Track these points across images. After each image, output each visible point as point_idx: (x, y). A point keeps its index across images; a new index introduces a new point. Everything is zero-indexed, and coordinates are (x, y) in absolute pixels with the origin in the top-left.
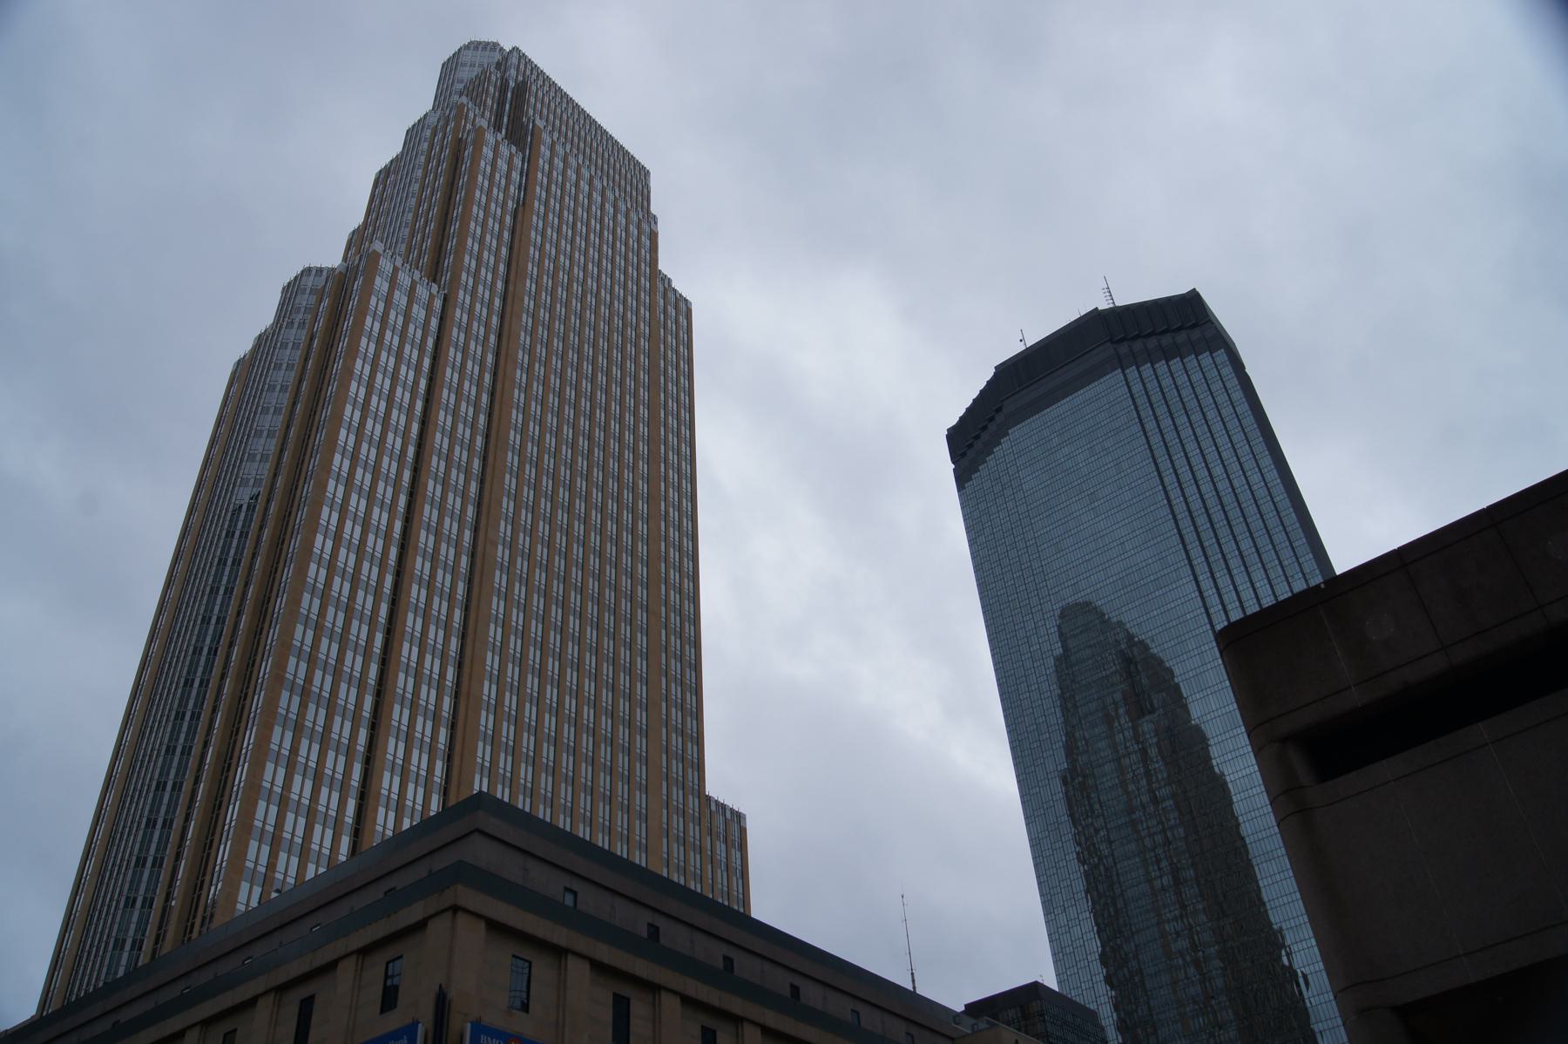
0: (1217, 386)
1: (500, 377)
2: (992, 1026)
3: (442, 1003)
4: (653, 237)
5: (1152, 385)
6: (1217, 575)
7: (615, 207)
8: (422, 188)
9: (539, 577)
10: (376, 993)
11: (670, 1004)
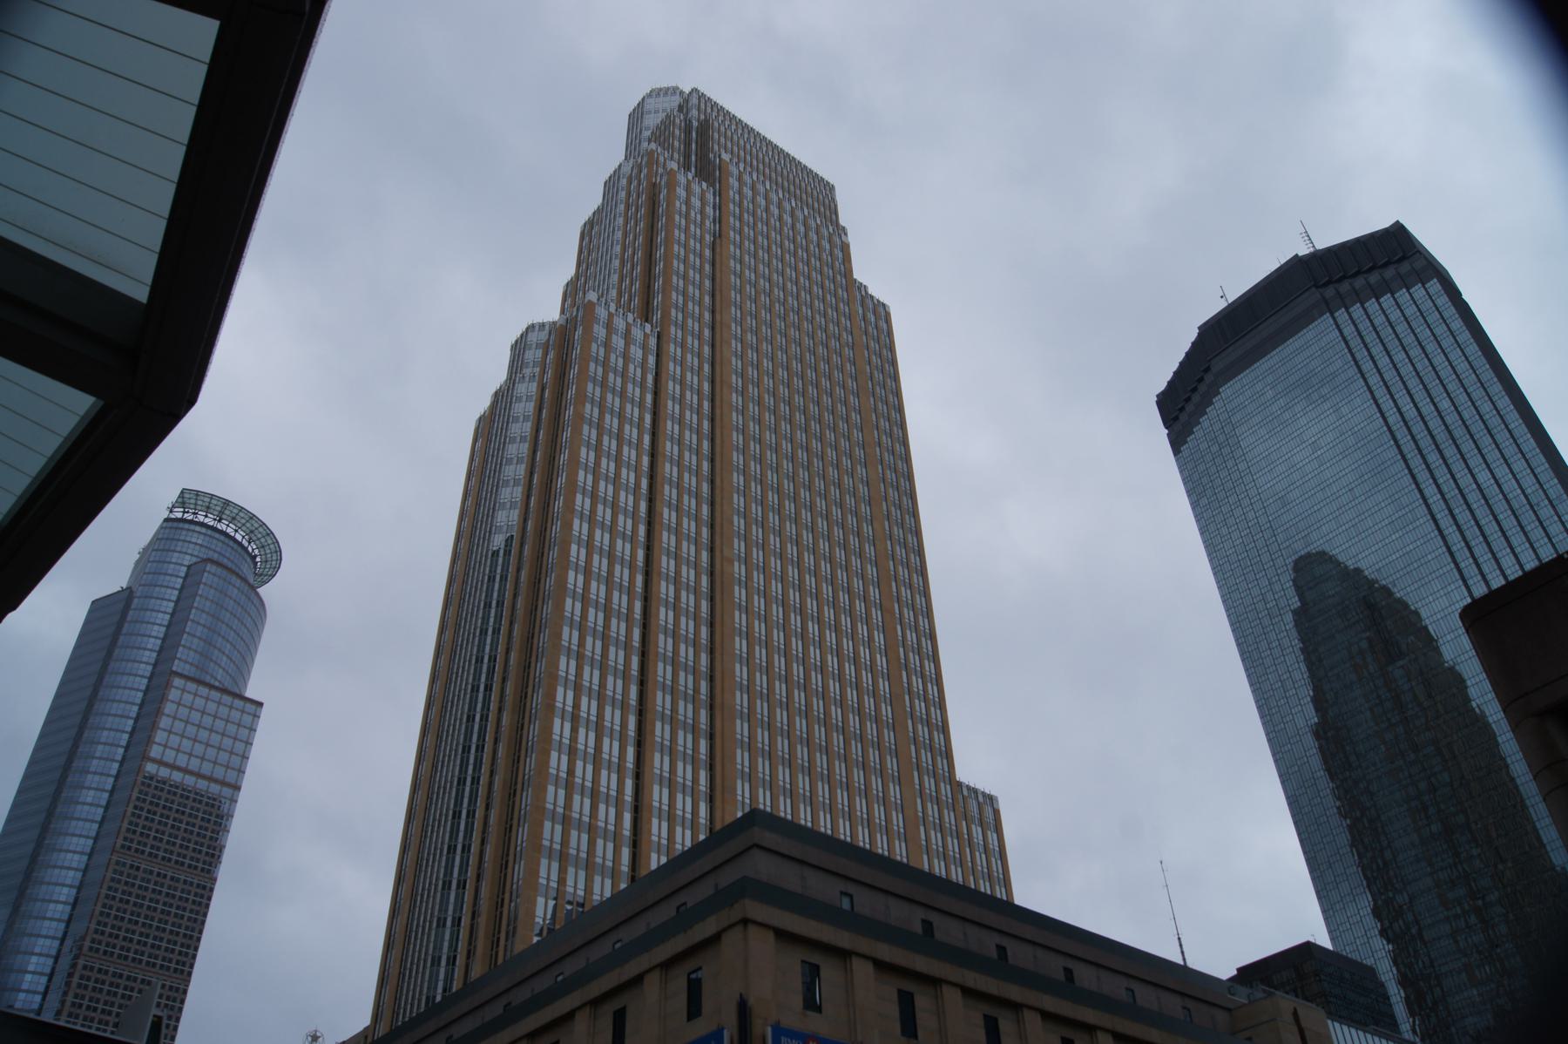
0: (1433, 318)
1: (718, 403)
2: (1270, 994)
3: (743, 1009)
4: (845, 248)
5: (1364, 326)
6: (1456, 511)
8: (625, 235)
9: (776, 588)
10: (681, 1001)
11: (952, 996)
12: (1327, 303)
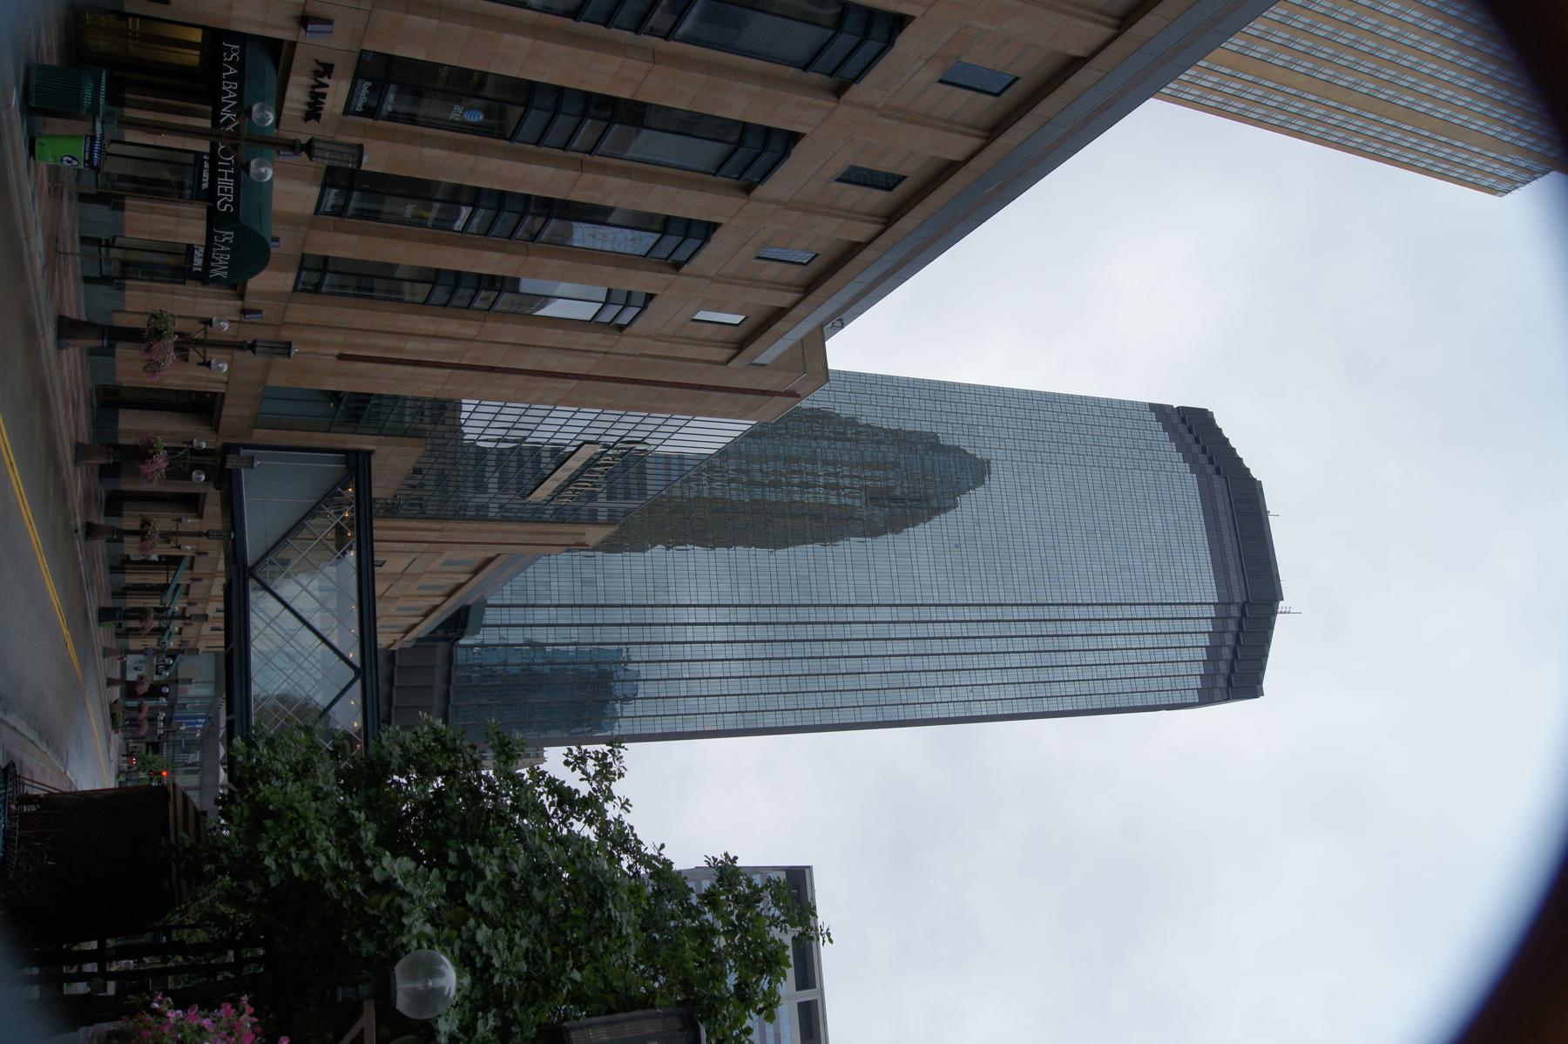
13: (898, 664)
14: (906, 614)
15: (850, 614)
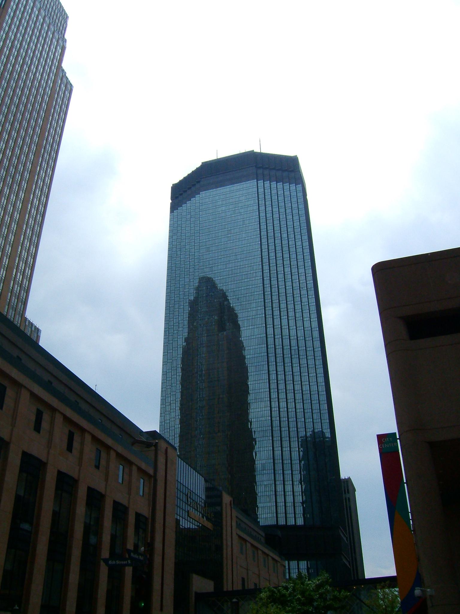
4: (63, 49)
7: (44, 19)
12: (257, 176)
13: (292, 323)
14: (270, 321)
15: (271, 346)
